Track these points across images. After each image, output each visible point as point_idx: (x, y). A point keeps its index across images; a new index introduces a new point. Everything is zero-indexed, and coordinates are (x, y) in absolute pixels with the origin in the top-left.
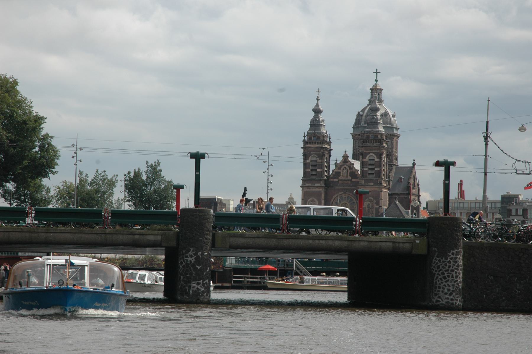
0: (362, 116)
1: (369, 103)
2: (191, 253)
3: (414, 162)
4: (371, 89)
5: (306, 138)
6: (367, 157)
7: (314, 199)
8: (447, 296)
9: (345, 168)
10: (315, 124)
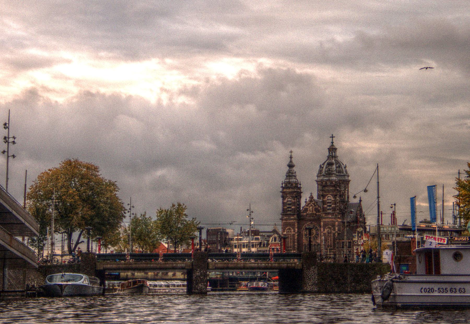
0: (323, 168)
1: (328, 158)
2: (198, 271)
3: (360, 200)
4: (328, 149)
5: (283, 185)
6: (326, 198)
7: (290, 228)
8: (310, 287)
9: (311, 205)
10: (290, 174)
